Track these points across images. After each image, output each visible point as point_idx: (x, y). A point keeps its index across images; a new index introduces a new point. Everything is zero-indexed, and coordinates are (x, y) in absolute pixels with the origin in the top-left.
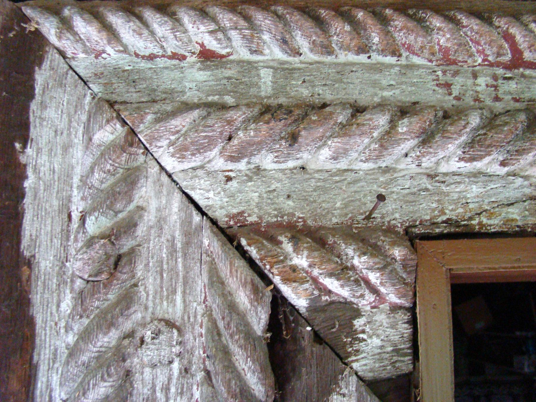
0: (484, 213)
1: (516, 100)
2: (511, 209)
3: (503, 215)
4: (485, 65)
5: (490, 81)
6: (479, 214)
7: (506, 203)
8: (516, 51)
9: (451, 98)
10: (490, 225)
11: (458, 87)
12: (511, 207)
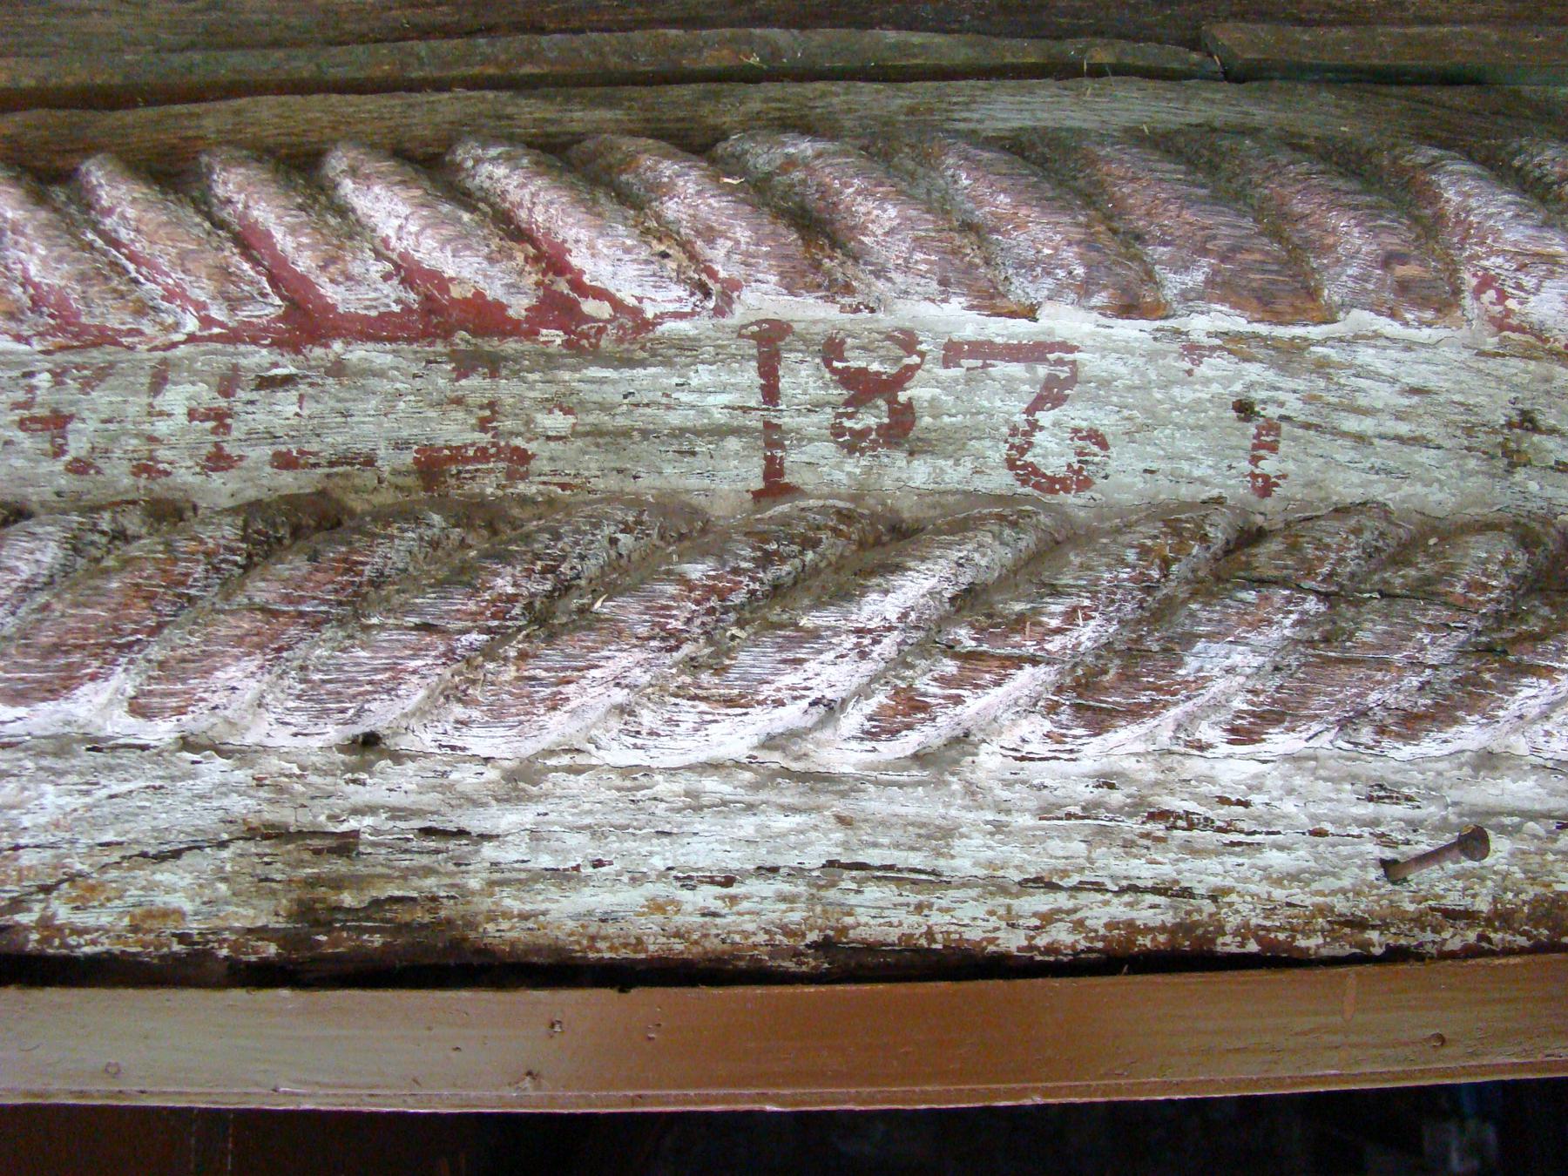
0: (66, 885)
1: (284, 462)
2: (165, 875)
3: (134, 893)
4: (211, 338)
5: (206, 395)
6: (46, 889)
7: (152, 851)
8: (280, 276)
9: (59, 466)
10: (80, 932)
11: (92, 425)
12: (166, 865)
